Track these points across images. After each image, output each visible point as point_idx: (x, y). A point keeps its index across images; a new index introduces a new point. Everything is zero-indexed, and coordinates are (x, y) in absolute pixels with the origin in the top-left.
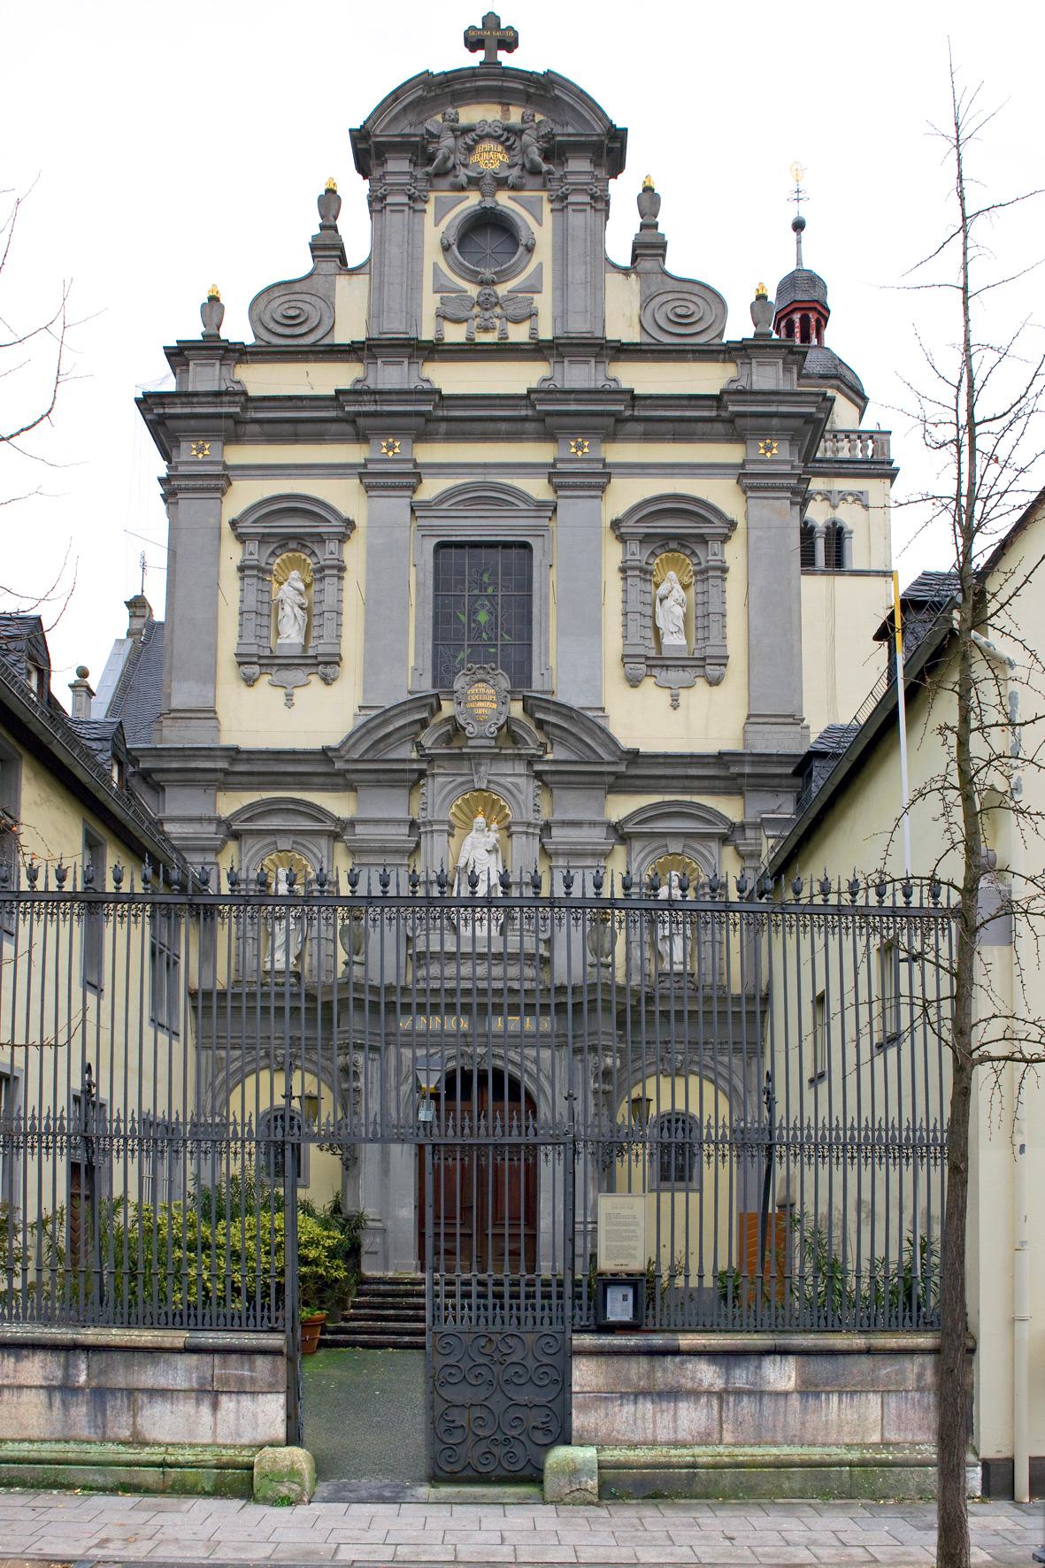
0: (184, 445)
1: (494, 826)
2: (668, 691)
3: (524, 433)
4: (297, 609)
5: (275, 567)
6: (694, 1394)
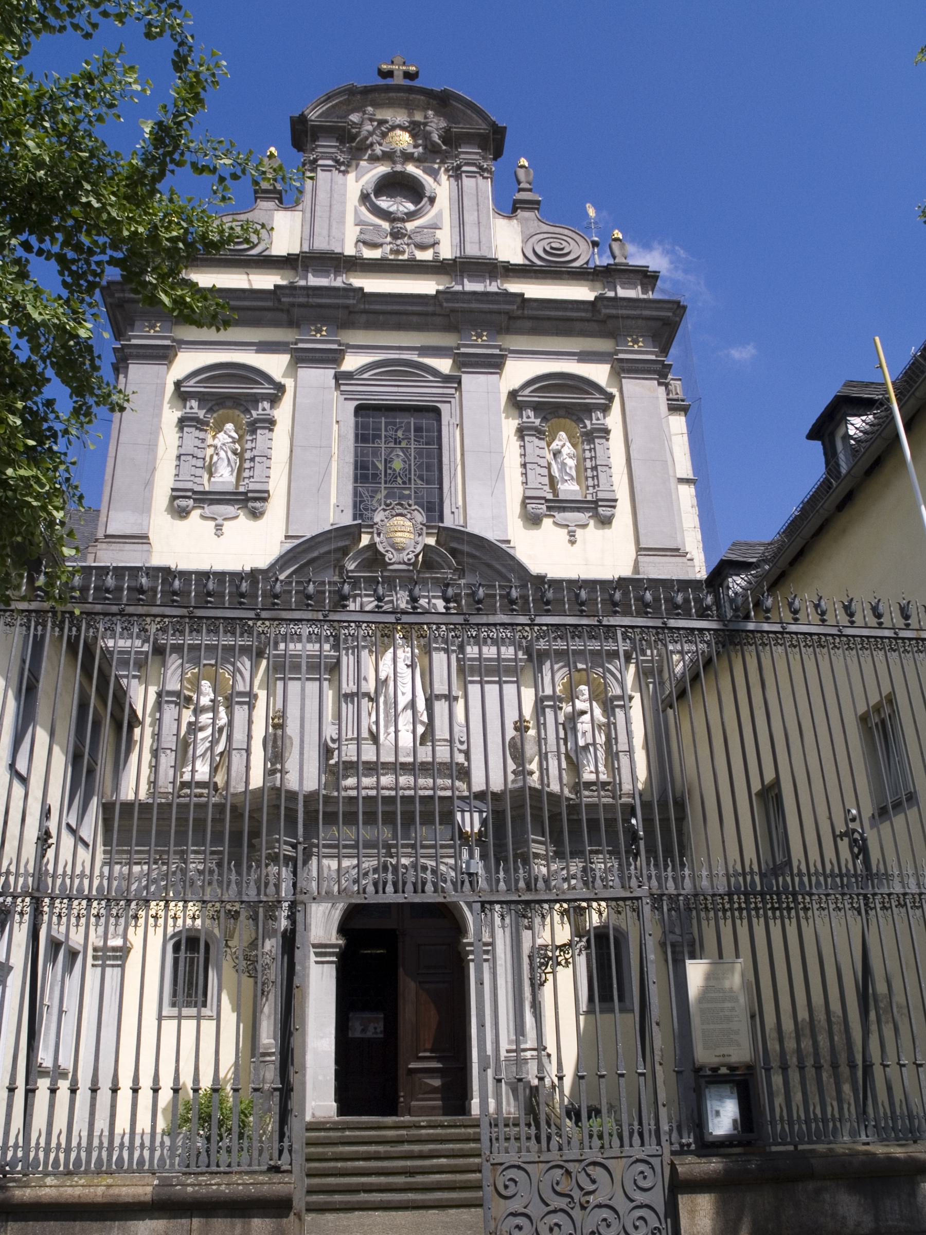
0: (137, 323)
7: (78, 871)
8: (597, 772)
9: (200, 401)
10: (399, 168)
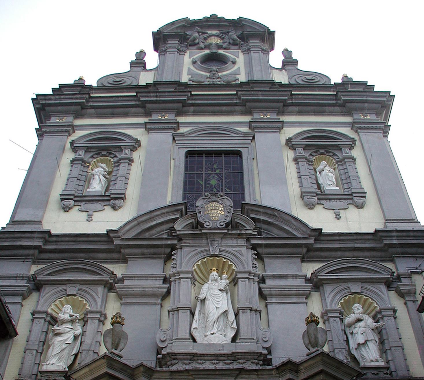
0: (52, 118)
1: (225, 276)
2: (332, 211)
3: (235, 111)
4: (101, 177)
5: (93, 162)
9: (88, 188)
10: (214, 51)
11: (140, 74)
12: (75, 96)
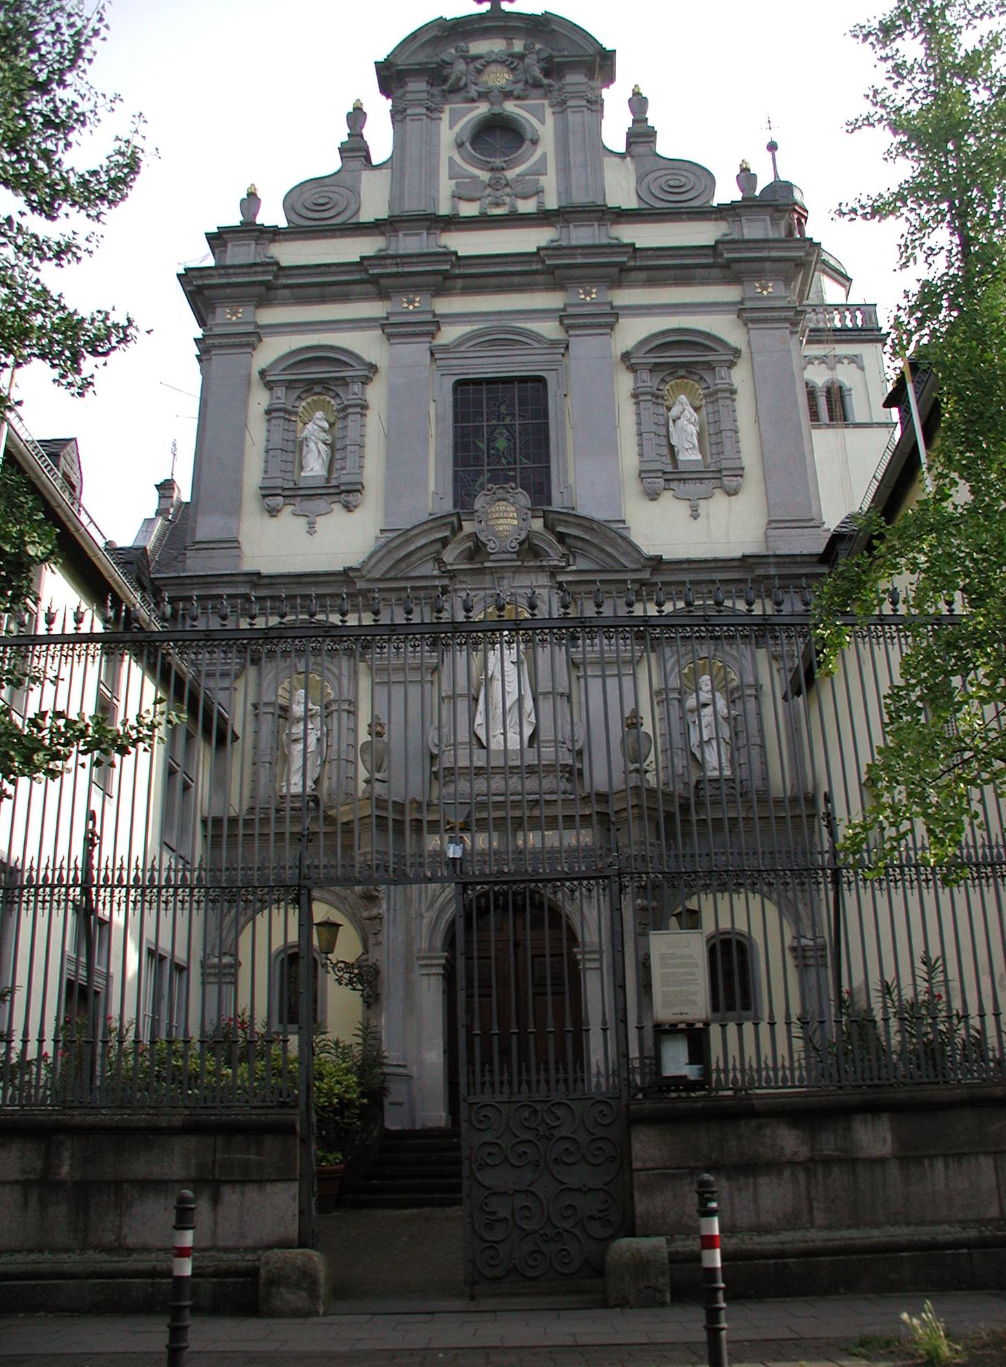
0: (219, 311)
4: (321, 445)
6: (774, 1166)
7: (118, 866)
8: (721, 769)
11: (359, 180)
12: (253, 270)
